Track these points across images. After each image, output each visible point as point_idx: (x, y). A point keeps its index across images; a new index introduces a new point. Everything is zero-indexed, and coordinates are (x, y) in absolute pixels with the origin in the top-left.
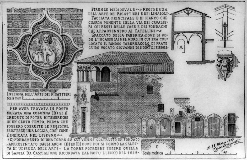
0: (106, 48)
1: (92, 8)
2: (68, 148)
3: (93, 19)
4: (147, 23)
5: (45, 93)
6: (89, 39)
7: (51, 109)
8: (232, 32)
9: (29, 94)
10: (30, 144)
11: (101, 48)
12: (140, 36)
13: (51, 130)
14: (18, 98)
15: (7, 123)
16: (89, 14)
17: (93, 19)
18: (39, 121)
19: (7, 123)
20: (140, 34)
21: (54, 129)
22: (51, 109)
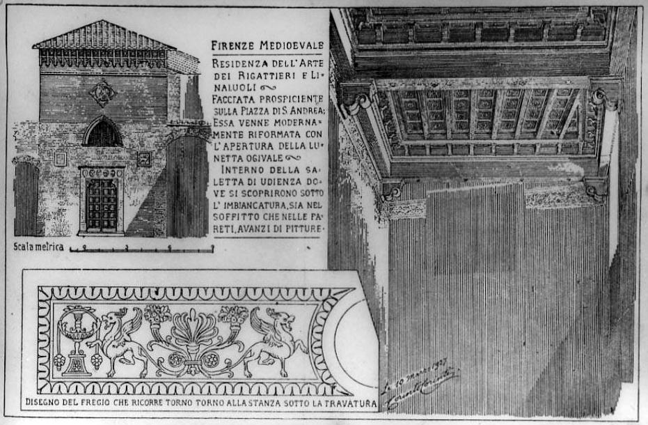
0: (256, 205)
1: (213, 42)
2: (320, 404)
3: (214, 47)
4: (222, 135)
5: (275, 226)
6: (249, 179)
7: (269, 228)
8: (612, 154)
9: (292, 216)
10: (237, 159)
11: (243, 159)
12: (256, 208)
13: (250, 191)
14: (44, 246)
15: (223, 172)
16: (250, 183)
17: (214, 47)
18: (218, 133)
19: (223, 172)
20: (256, 203)
21: (222, 117)
22: (269, 228)
